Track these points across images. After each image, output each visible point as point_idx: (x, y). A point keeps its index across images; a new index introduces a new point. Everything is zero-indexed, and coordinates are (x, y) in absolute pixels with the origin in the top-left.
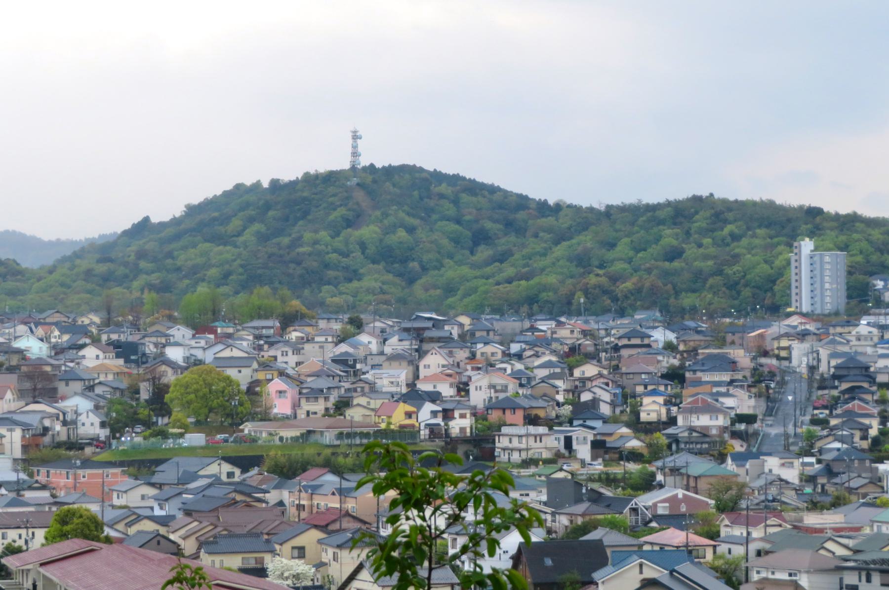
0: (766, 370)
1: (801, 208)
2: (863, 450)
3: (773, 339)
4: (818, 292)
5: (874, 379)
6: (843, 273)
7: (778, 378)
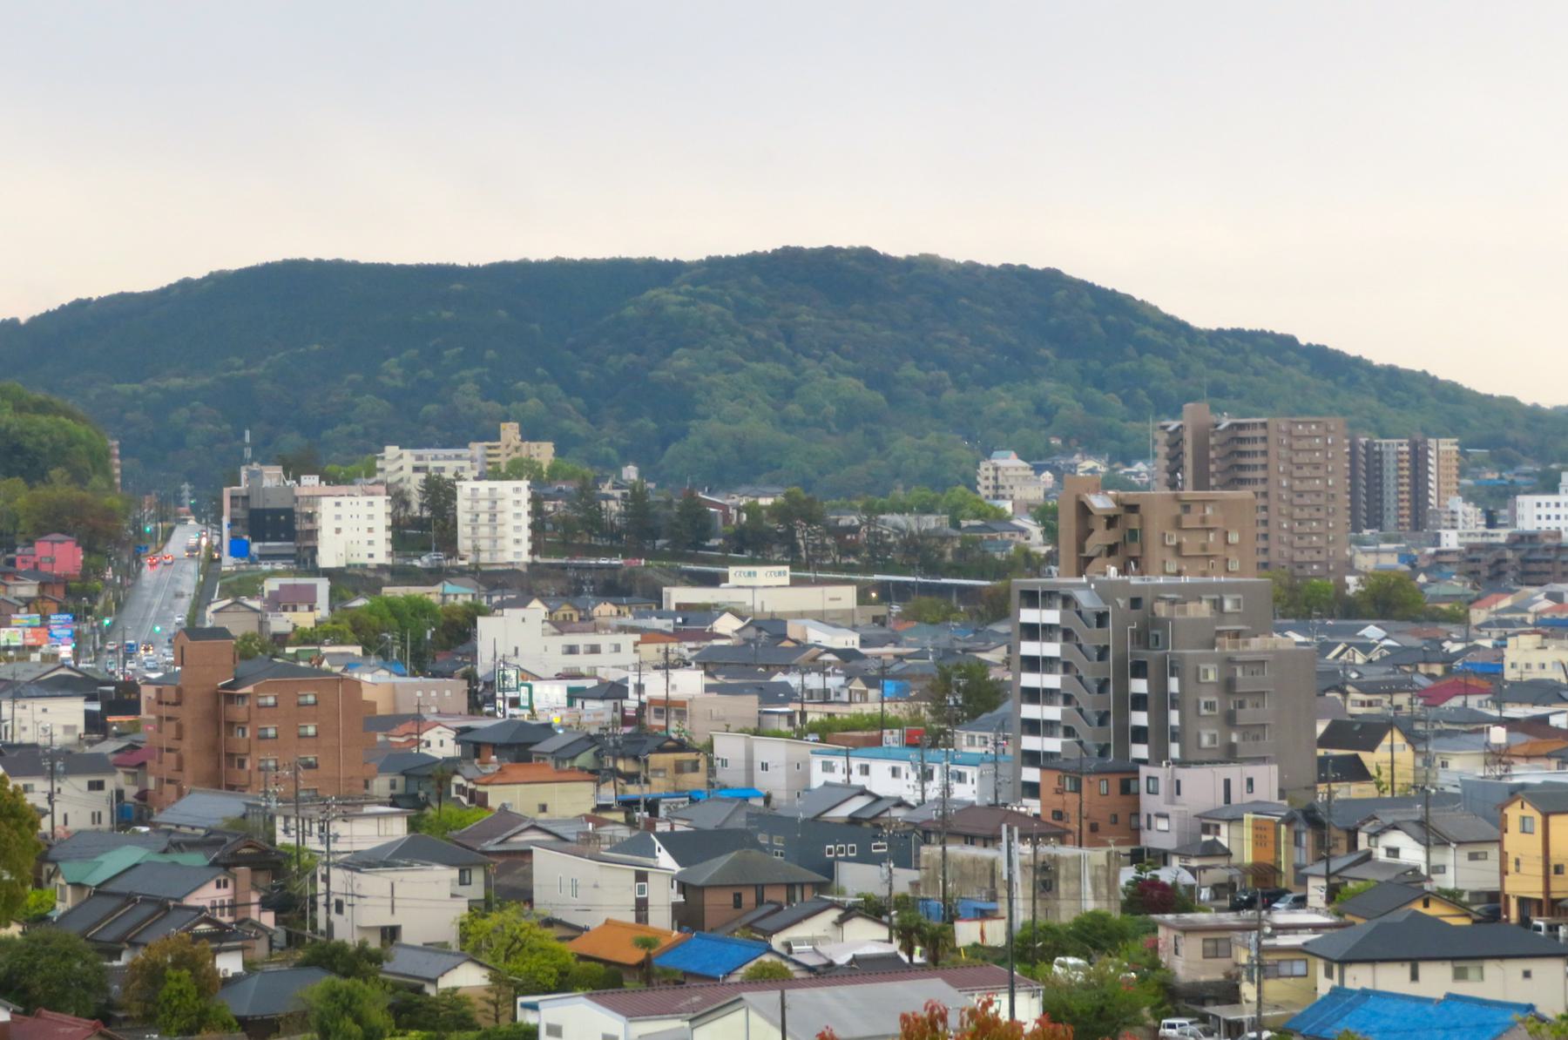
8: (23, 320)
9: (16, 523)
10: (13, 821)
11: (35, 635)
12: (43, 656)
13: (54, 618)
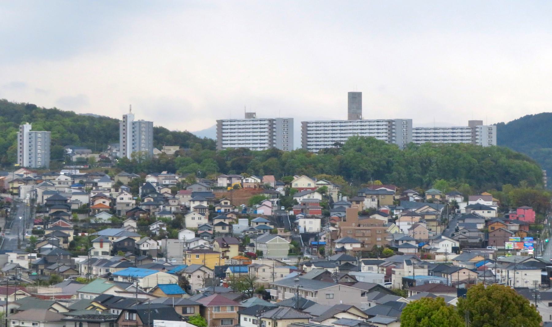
0: (5, 201)
1: (23, 104)
2: (65, 249)
3: (9, 182)
4: (33, 155)
5: (70, 207)
6: (48, 144)
7: (12, 206)
8: (506, 123)
9: (509, 202)
10: (531, 318)
11: (518, 245)
12: (521, 253)
13: (526, 239)
